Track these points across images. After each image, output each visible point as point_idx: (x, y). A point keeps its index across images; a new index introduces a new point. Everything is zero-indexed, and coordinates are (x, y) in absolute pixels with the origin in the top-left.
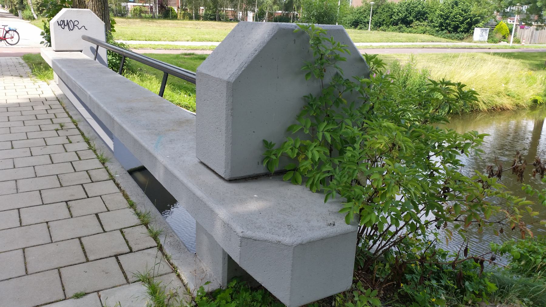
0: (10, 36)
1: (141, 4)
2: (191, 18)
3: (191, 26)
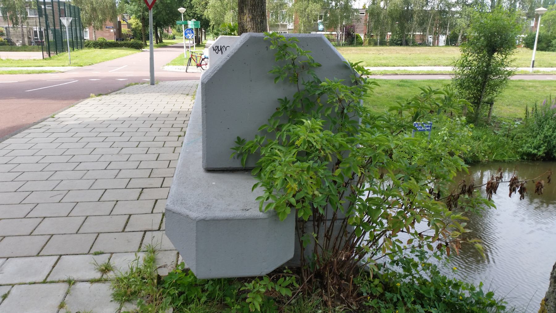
0: (205, 63)
1: (328, 33)
2: (376, 44)
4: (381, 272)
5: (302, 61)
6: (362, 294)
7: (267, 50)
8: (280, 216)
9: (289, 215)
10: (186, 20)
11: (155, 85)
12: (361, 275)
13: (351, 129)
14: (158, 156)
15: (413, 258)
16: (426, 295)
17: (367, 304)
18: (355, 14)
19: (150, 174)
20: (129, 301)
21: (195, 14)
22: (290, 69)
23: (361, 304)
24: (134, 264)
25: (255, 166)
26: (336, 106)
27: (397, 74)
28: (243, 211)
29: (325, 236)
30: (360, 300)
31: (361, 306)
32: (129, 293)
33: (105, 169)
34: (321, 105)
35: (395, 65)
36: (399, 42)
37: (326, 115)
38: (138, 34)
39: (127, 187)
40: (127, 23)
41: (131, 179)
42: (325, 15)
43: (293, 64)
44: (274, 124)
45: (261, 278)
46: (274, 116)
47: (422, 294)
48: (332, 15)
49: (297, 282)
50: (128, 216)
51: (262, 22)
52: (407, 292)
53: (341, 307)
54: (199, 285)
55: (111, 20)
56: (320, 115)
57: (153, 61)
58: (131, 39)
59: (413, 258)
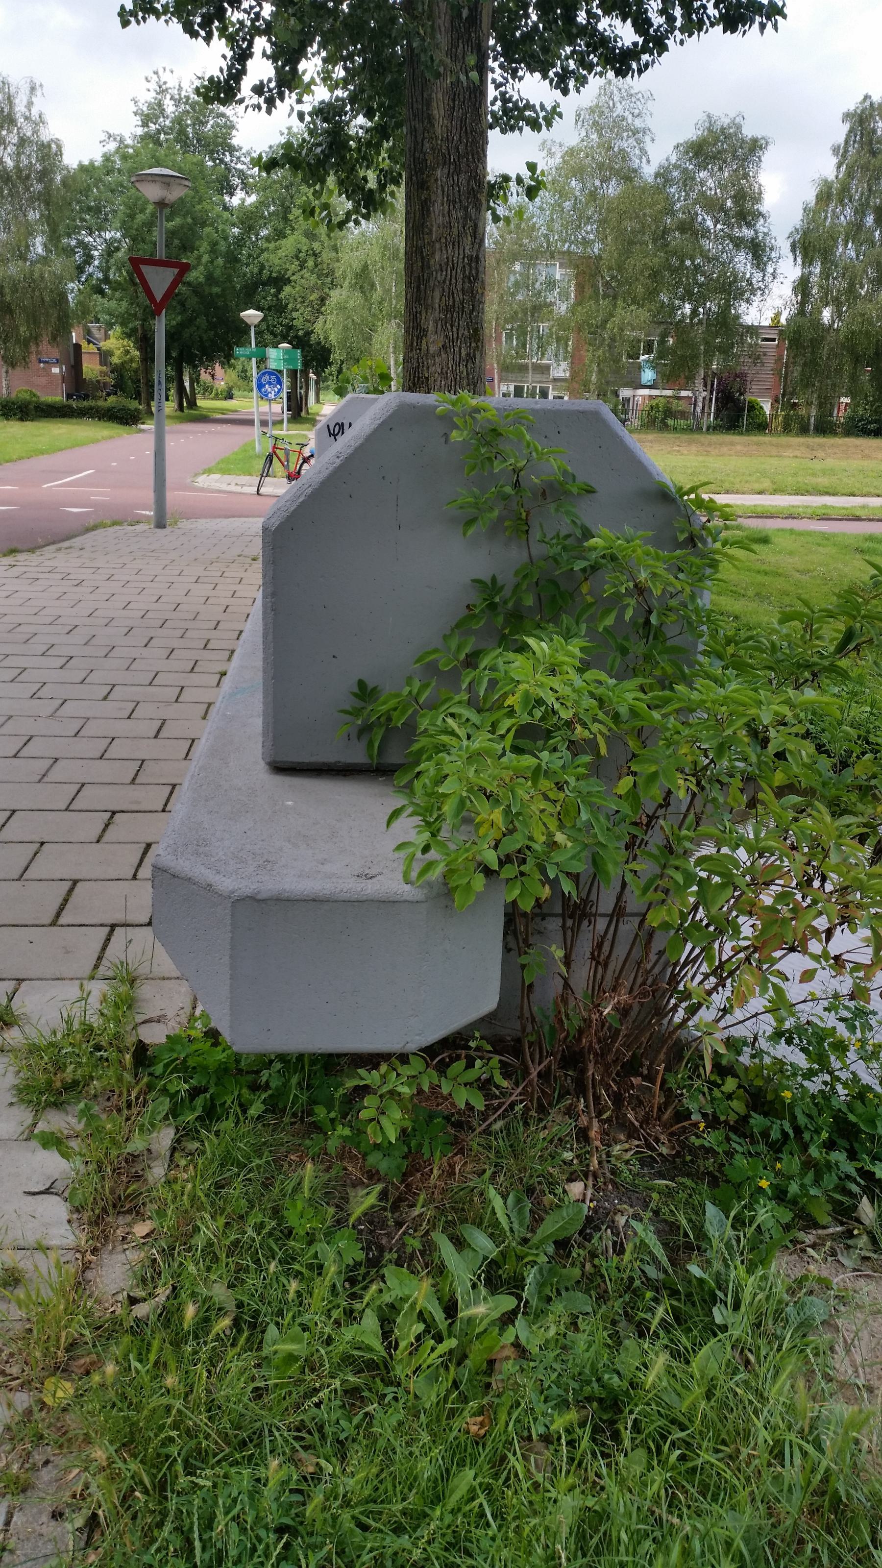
1: (669, 393)
2: (804, 430)
3: (798, 453)
4: (745, 1059)
5: (543, 477)
6: (688, 1115)
7: (446, 442)
8: (457, 897)
9: (480, 896)
10: (262, 344)
11: (169, 529)
12: (686, 1065)
13: (669, 670)
14: (161, 727)
15: (834, 1028)
16: (863, 1127)
17: (698, 1142)
18: (749, 340)
19: (136, 775)
20: (57, 1105)
21: (290, 328)
22: (506, 497)
23: (683, 1145)
24: (74, 1010)
25: (401, 762)
26: (628, 605)
27: (858, 519)
28: (360, 880)
29: (593, 958)
30: (684, 1130)
31: (683, 1149)
32: (58, 1084)
33: (15, 756)
34: (589, 599)
35: (856, 492)
36: (872, 426)
37: (601, 630)
38: (129, 383)
39: (71, 808)
40: (99, 349)
41: (83, 785)
42: (662, 342)
43: (517, 485)
44: (459, 648)
45: (404, 1058)
46: (461, 626)
47: (855, 1125)
48: (682, 342)
49: (506, 1075)
50: (69, 883)
51: (471, 358)
52: (809, 1116)
53: (627, 1146)
54: (247, 1072)
55: (54, 338)
56: (584, 627)
57: (163, 460)
58: (108, 395)
59: (834, 1028)
